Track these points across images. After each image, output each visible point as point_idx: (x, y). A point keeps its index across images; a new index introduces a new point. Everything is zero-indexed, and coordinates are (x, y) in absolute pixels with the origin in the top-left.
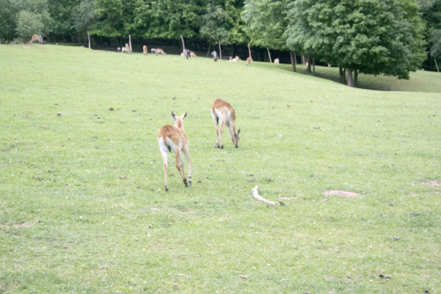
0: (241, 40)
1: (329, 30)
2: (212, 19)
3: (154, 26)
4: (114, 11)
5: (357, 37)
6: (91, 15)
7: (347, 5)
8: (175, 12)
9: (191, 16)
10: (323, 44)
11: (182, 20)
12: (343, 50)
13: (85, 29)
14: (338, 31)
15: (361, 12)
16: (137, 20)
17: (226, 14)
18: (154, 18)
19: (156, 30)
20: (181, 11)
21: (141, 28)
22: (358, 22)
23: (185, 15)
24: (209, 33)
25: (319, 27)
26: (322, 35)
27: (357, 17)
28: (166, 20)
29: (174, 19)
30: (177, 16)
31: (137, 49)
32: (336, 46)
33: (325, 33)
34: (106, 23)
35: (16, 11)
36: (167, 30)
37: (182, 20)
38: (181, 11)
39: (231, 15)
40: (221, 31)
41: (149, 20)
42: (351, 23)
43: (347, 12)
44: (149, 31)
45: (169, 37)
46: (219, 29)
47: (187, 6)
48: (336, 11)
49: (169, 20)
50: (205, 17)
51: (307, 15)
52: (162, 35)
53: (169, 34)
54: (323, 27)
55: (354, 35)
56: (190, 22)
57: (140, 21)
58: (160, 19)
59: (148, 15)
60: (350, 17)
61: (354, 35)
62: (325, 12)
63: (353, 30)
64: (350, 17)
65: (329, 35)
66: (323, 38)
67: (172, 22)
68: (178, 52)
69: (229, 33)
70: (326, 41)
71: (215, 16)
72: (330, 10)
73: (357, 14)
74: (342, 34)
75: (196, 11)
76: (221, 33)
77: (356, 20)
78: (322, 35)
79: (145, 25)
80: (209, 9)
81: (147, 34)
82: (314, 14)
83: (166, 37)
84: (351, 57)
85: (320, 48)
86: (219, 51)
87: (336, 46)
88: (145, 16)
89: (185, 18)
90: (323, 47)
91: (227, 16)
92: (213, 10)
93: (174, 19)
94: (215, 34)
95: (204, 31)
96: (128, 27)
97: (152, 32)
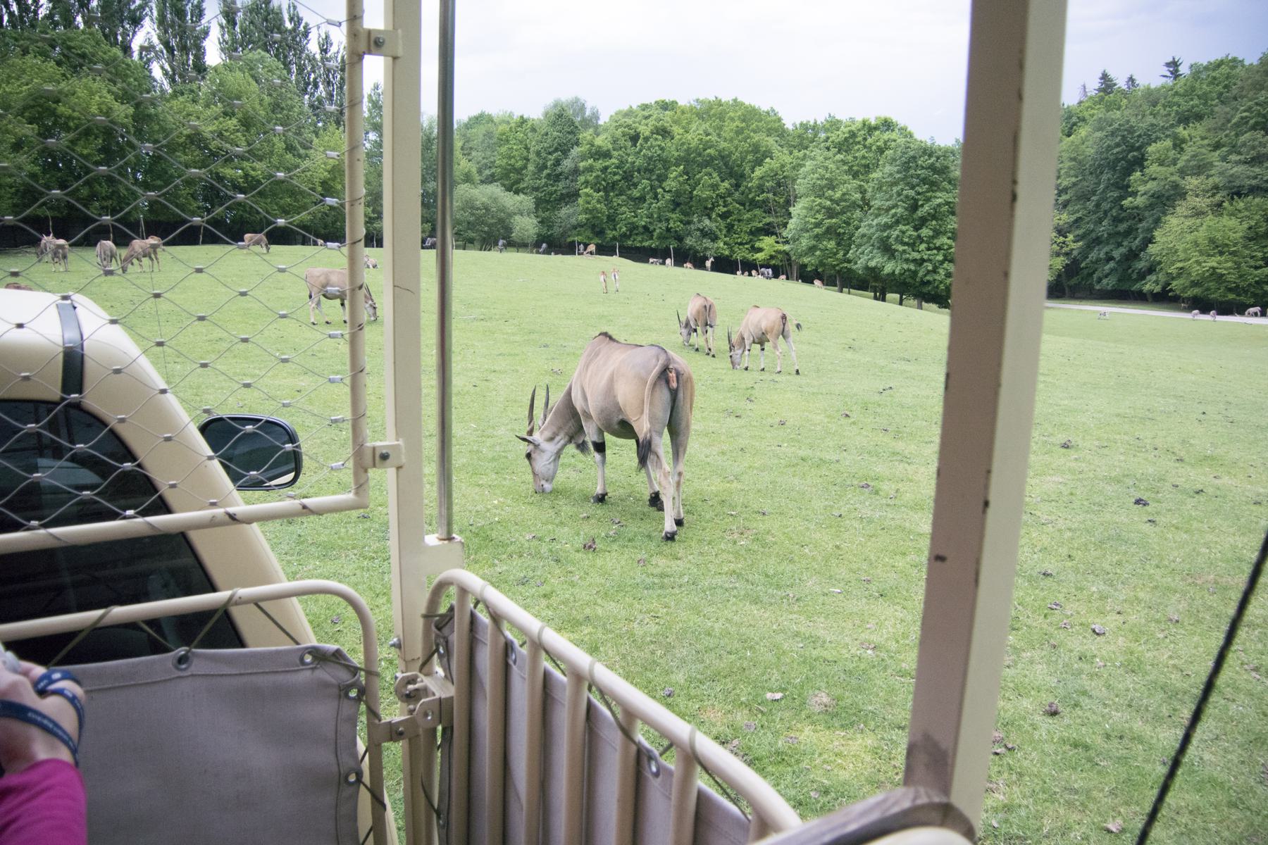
0: (727, 253)
1: (916, 255)
2: (698, 229)
3: (637, 234)
4: (598, 217)
5: (945, 265)
6: (573, 221)
7: (934, 230)
8: (660, 221)
9: (678, 226)
10: (909, 270)
11: (668, 230)
12: (928, 278)
13: (563, 234)
14: (925, 257)
15: (949, 238)
16: (621, 228)
17: (713, 226)
18: (637, 227)
19: (639, 238)
20: (668, 220)
21: (624, 236)
22: (947, 249)
23: (671, 225)
24: (695, 244)
25: (904, 251)
26: (907, 260)
27: (946, 244)
28: (651, 228)
29: (660, 228)
30: (663, 225)
31: (679, 262)
32: (921, 274)
33: (911, 258)
34: (586, 229)
35: (510, 215)
36: (652, 239)
37: (668, 230)
38: (668, 220)
39: (717, 227)
40: (707, 243)
41: (633, 228)
42: (939, 249)
43: (933, 237)
44: (632, 239)
45: (653, 246)
46: (704, 241)
47: (674, 216)
48: (922, 235)
49: (655, 229)
50: (693, 227)
51: (888, 237)
52: (646, 244)
53: (654, 244)
54: (908, 251)
55: (942, 263)
56: (676, 231)
57: (624, 229)
58: (645, 227)
59: (633, 223)
60: (938, 242)
61: (942, 263)
62: (911, 235)
63: (940, 258)
64: (938, 242)
65: (914, 261)
66: (907, 263)
67: (658, 231)
68: (733, 272)
69: (716, 245)
70: (912, 267)
71: (701, 228)
72: (916, 234)
73: (944, 240)
74: (929, 260)
75: (681, 222)
76: (707, 245)
77: (946, 247)
78: (907, 260)
79: (628, 233)
80: (695, 220)
81: (630, 243)
82: (898, 236)
83: (650, 246)
84: (937, 287)
85: (903, 274)
86: (300, 228)
87: (921, 274)
88: (629, 224)
89: (671, 228)
90: (907, 273)
91: (714, 229)
92: (699, 221)
93: (660, 228)
94: (701, 244)
95: (689, 241)
96: (610, 234)
97: (634, 240)
